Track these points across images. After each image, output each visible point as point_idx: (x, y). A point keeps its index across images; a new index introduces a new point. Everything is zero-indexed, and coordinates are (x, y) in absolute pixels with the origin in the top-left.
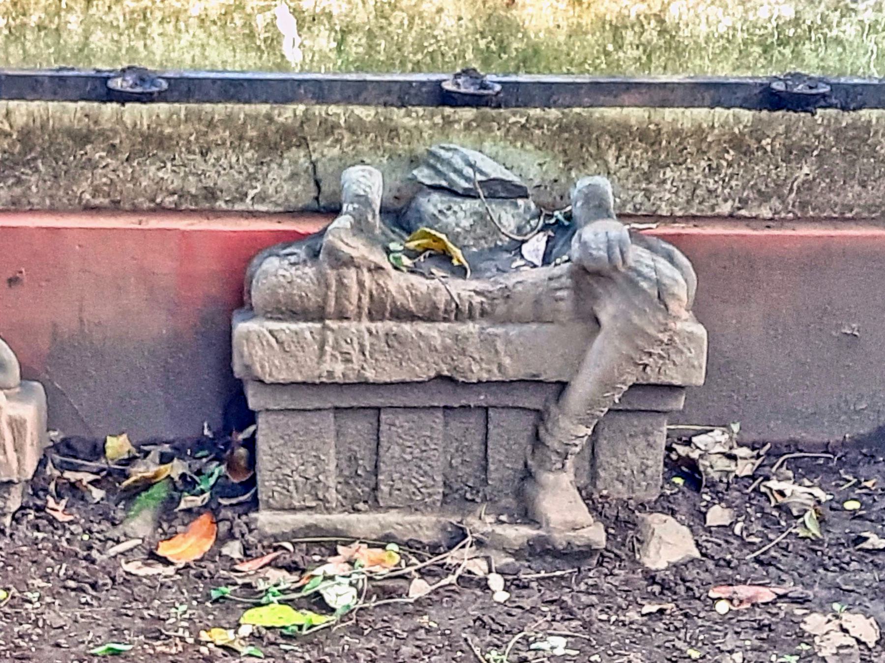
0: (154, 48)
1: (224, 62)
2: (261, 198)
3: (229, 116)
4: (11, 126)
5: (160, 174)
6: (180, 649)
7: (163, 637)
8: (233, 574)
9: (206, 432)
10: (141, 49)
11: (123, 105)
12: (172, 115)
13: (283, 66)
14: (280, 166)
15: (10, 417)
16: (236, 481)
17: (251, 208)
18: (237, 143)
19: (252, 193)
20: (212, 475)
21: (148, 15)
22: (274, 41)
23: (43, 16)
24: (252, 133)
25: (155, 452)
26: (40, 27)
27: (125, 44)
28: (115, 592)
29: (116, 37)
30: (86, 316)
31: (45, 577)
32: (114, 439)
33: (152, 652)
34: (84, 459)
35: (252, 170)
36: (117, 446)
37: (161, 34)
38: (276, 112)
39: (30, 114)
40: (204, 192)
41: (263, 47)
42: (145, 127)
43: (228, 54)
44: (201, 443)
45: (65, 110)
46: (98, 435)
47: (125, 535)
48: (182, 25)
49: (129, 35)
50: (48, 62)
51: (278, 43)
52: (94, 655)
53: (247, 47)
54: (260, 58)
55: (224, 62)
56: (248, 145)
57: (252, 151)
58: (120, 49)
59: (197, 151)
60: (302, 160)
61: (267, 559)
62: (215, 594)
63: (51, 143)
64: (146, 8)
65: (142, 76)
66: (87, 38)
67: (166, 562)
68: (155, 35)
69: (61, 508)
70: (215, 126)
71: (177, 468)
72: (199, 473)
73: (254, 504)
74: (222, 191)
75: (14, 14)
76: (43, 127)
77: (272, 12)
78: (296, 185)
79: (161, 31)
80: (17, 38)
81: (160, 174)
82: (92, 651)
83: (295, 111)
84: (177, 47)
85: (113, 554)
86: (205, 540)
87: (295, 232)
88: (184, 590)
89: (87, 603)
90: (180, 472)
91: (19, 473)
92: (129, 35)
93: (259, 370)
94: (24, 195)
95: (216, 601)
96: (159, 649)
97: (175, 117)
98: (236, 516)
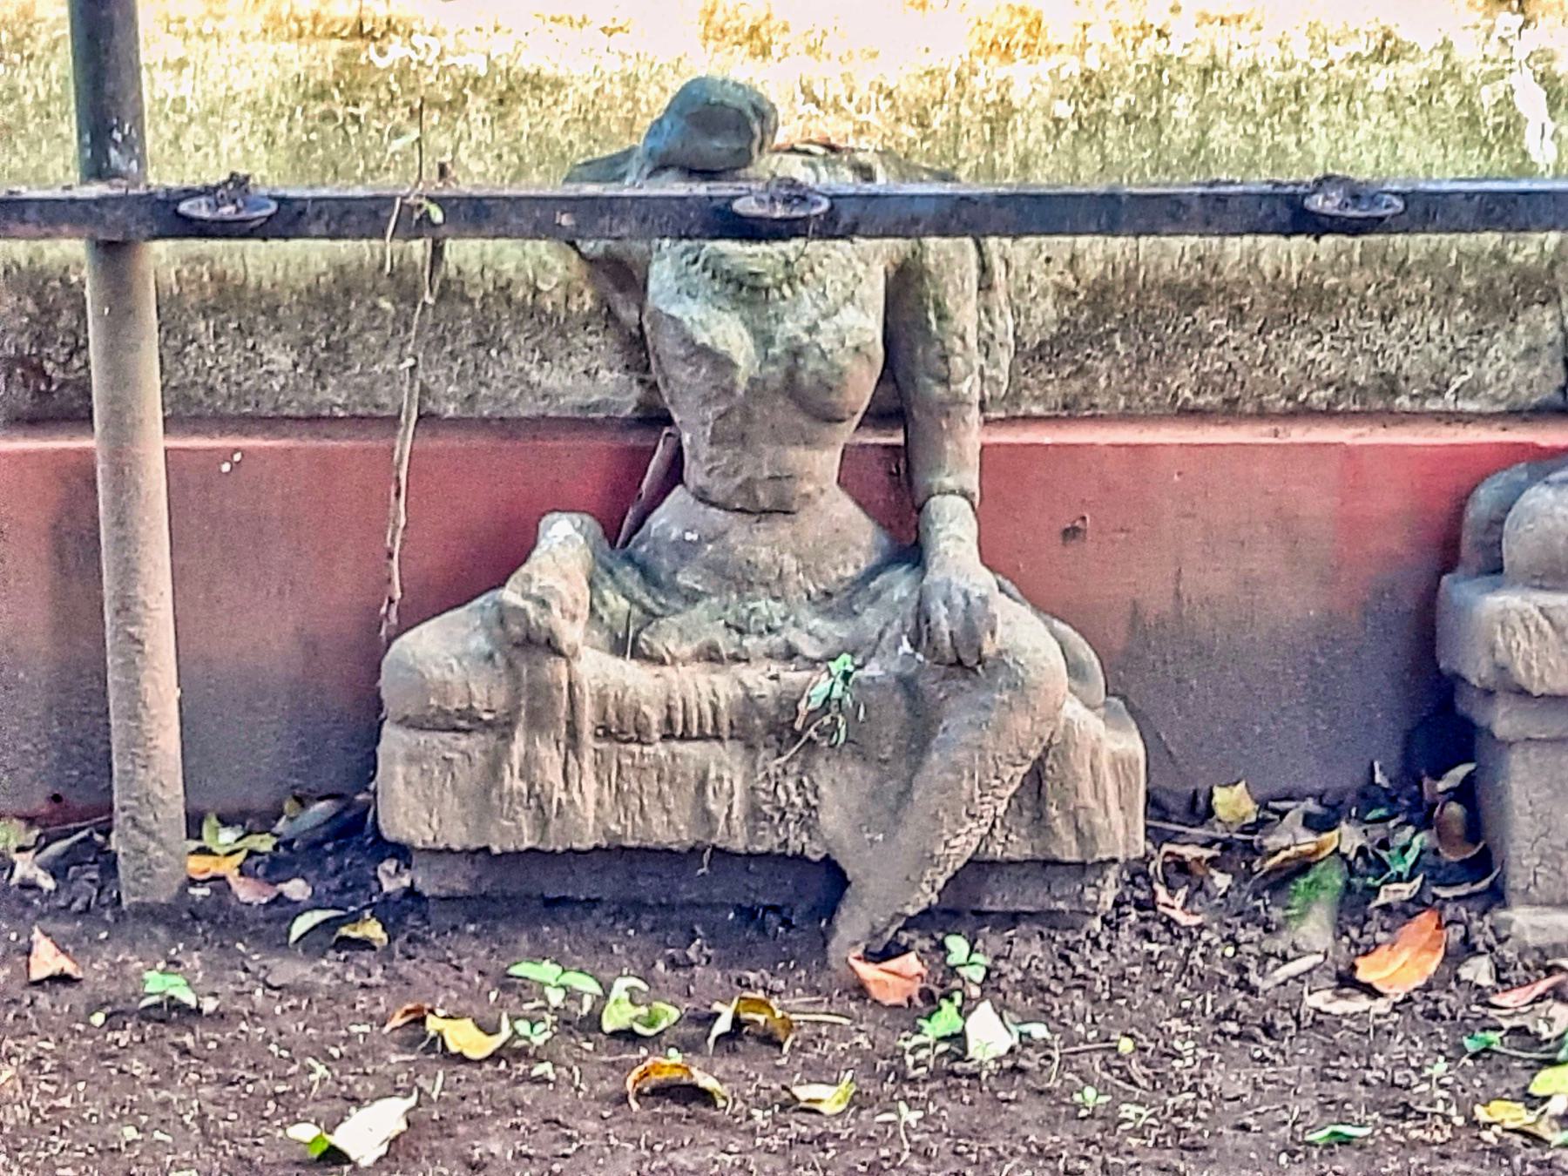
0: (1313, 145)
1: (1428, 166)
2: (1471, 390)
3: (1432, 255)
4: (1078, 281)
5: (1311, 354)
6: (1448, 1134)
7: (1413, 1115)
8: (1492, 1013)
9: (1378, 778)
10: (1292, 148)
11: (1317, 239)
12: (1339, 255)
13: (1525, 168)
14: (1510, 335)
15: (1113, 753)
16: (1452, 858)
17: (1452, 408)
18: (1442, 300)
19: (1457, 381)
20: (1405, 849)
21: (1304, 92)
22: (1511, 128)
23: (1133, 98)
24: (1469, 283)
25: (1296, 811)
26: (1129, 117)
27: (1266, 143)
28: (1304, 1041)
29: (1251, 129)
30: (1186, 587)
31: (1184, 1014)
32: (1225, 791)
33: (1402, 1139)
34: (1178, 823)
35: (1462, 344)
36: (1233, 803)
37: (1324, 124)
38: (1512, 246)
39: (1110, 259)
40: (1379, 381)
41: (1492, 139)
42: (1294, 277)
43: (1434, 153)
44: (1368, 797)
45: (1165, 251)
46: (1203, 786)
47: (1295, 947)
48: (1358, 106)
49: (1271, 126)
50: (1143, 174)
51: (1517, 131)
52: (1310, 1144)
53: (1465, 140)
54: (1488, 157)
55: (1428, 166)
56: (1460, 301)
57: (1468, 312)
58: (1257, 150)
59: (1376, 313)
60: (1548, 326)
61: (1541, 987)
62: (1471, 1046)
63: (1140, 307)
64: (1299, 82)
65: (1356, 194)
66: (1204, 133)
67: (1372, 992)
68: (1315, 125)
69: (1178, 904)
70: (1409, 273)
71: (1349, 837)
72: (1384, 845)
73: (1497, 896)
74: (1407, 379)
75: (1086, 98)
76: (1128, 281)
77: (1506, 81)
78: (1530, 367)
79: (1324, 117)
80: (1092, 136)
81: (1311, 354)
82: (1309, 1138)
83: (1542, 244)
84: (1351, 145)
85: (1280, 980)
86: (1427, 956)
87: (1534, 446)
88: (1417, 1039)
89: (1263, 1059)
90: (1358, 844)
91: (1127, 846)
92: (1271, 126)
93: (1523, 673)
94: (1086, 391)
95: (1474, 1057)
96: (1414, 1134)
97: (1343, 258)
98: (1474, 915)
